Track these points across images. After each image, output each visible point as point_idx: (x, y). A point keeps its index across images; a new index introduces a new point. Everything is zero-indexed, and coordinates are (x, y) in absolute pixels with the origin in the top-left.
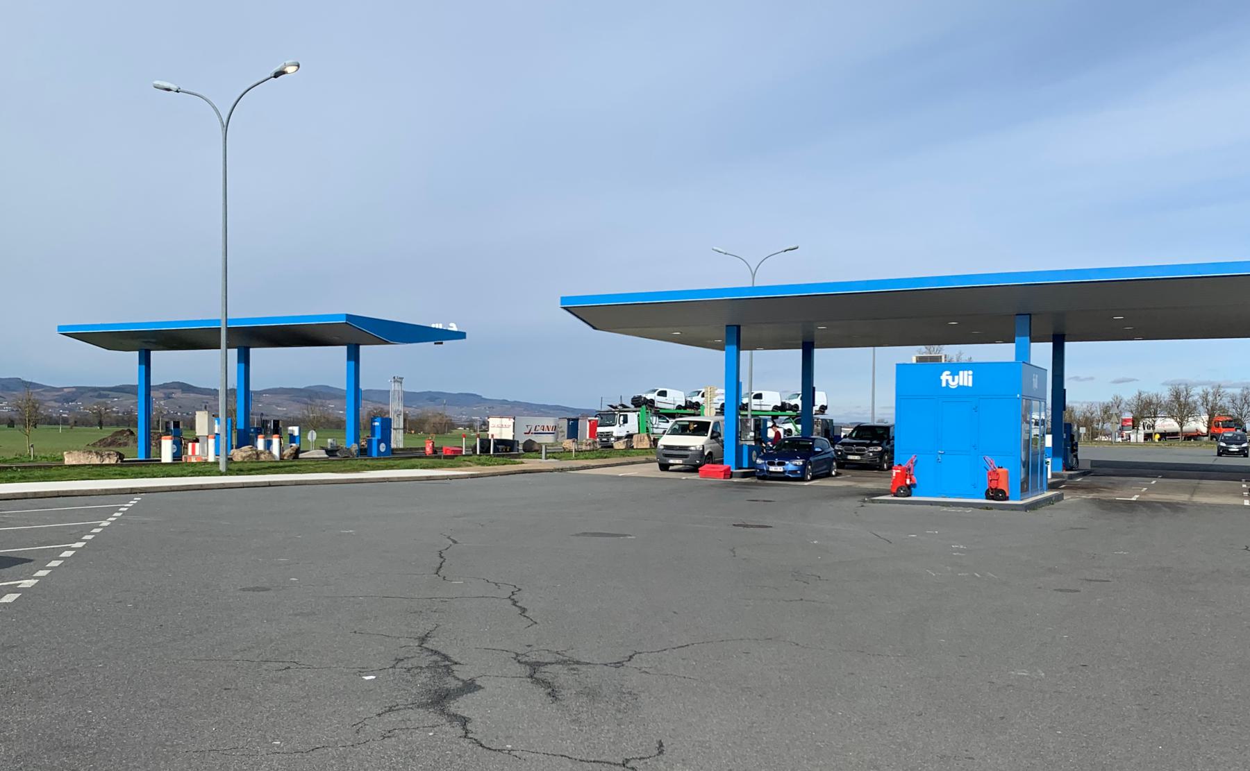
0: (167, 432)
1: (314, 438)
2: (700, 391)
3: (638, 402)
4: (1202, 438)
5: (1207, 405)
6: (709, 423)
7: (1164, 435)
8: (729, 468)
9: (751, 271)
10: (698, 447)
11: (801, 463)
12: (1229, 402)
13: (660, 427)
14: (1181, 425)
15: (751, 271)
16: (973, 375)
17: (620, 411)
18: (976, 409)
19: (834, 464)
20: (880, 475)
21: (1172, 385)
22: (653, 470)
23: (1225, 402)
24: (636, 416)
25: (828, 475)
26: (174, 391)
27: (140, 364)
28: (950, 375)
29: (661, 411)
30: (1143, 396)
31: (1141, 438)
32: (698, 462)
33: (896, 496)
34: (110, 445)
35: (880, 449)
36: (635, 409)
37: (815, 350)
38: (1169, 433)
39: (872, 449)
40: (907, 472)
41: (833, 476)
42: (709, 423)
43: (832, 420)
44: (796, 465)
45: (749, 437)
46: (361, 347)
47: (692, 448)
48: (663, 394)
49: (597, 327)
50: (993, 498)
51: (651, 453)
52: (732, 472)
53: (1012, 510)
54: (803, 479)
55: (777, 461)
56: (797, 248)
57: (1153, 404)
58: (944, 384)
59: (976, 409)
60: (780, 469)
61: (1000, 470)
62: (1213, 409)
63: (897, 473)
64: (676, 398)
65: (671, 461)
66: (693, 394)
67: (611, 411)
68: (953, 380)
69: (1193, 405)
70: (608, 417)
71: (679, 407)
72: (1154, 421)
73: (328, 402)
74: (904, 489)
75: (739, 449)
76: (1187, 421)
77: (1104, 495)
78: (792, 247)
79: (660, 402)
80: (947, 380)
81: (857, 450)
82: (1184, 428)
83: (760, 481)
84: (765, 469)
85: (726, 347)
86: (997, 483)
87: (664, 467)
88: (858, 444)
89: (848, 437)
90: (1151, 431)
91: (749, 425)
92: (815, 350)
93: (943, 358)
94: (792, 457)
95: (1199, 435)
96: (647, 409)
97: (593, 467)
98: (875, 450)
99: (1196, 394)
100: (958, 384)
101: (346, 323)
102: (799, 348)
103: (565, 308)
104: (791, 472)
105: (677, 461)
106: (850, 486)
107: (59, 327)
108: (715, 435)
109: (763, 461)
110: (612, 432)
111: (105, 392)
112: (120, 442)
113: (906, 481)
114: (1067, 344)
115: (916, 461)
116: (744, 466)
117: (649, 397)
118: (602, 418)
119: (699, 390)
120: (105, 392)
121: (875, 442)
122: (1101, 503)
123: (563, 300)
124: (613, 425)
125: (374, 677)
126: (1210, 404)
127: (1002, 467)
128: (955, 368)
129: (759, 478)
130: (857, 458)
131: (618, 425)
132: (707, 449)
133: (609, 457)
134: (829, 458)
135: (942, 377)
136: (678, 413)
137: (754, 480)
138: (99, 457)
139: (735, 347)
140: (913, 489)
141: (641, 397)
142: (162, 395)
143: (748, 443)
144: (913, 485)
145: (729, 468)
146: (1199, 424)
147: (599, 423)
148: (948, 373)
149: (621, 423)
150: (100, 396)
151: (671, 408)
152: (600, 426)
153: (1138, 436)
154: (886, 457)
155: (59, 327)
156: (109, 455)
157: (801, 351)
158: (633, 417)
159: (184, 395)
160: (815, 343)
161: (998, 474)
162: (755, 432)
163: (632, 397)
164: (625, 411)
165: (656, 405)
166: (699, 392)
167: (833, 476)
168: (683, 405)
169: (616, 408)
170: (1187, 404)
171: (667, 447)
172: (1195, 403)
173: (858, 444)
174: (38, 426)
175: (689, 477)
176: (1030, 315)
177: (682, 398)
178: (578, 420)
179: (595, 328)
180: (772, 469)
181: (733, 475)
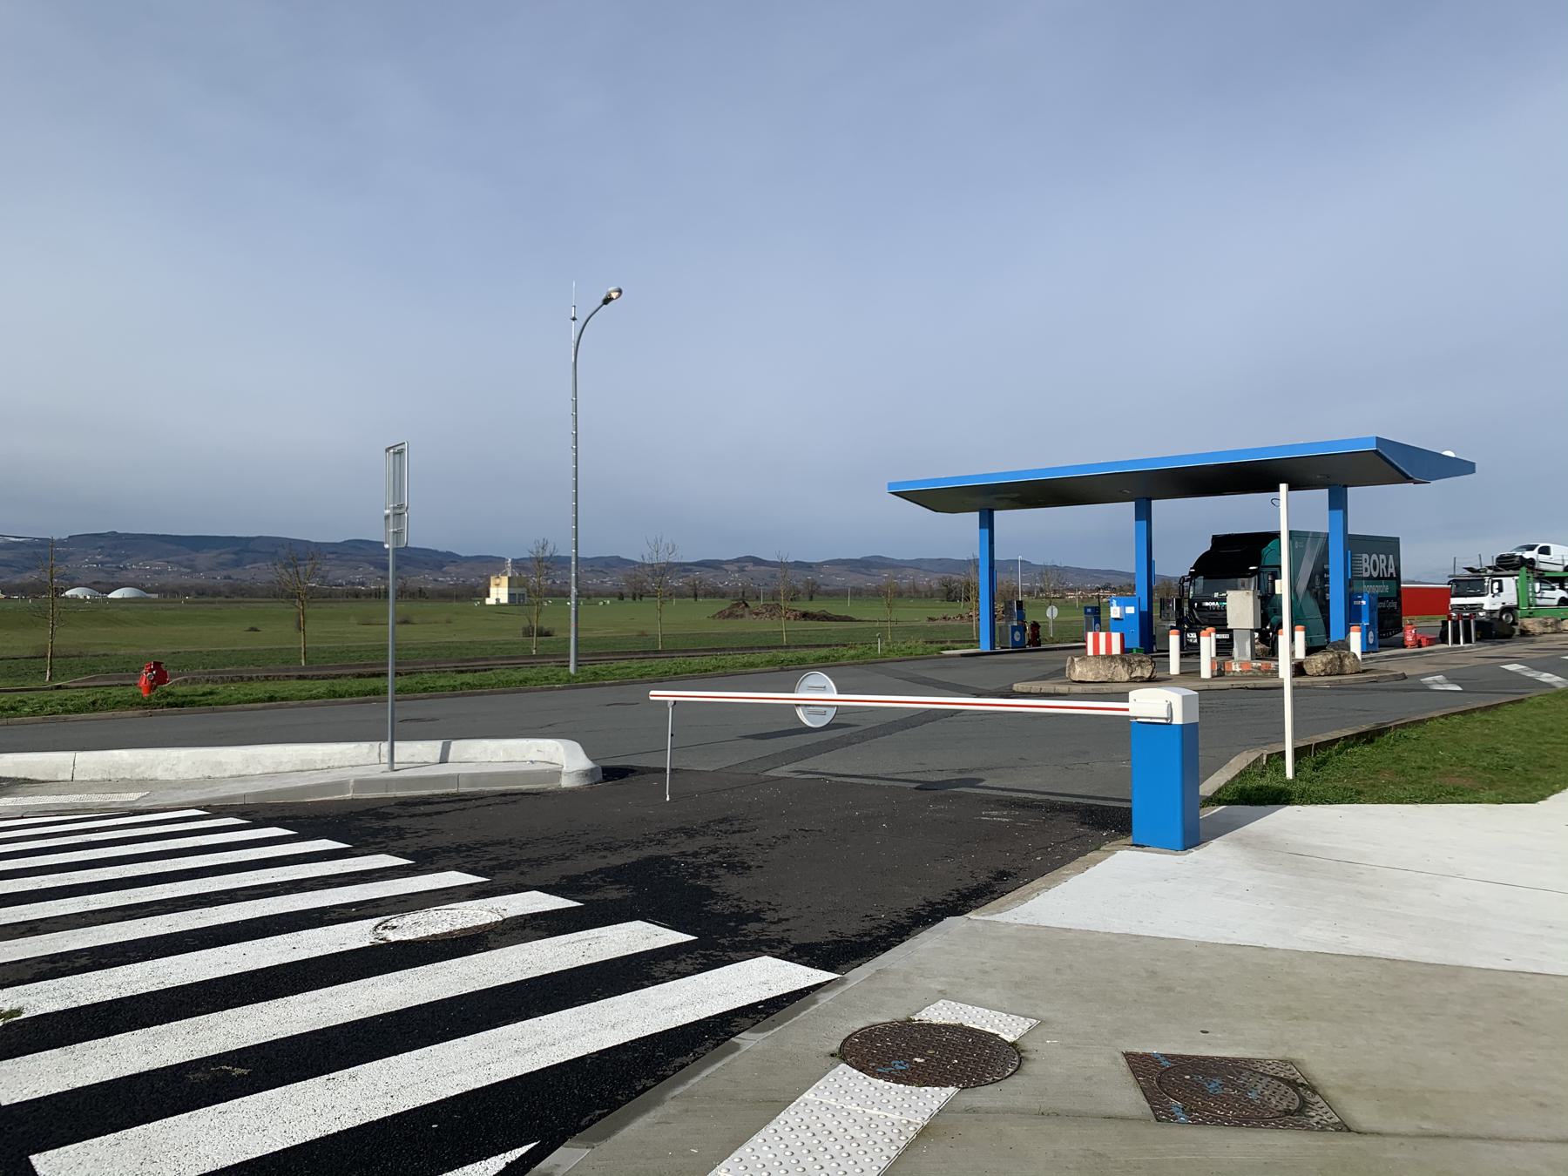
1: (1055, 615)
2: (1536, 546)
13: (1545, 596)
26: (747, 564)
27: (981, 527)
29: (1547, 575)
34: (728, 616)
46: (995, 512)
70: (1473, 583)
73: (882, 571)
101: (1376, 452)
102: (1144, 520)
103: (893, 493)
107: (889, 484)
110: (1482, 605)
111: (690, 567)
112: (738, 613)
117: (1528, 555)
120: (690, 567)
123: (890, 485)
124: (1483, 595)
131: (1490, 595)
138: (1126, 666)
141: (1513, 556)
142: (736, 568)
147: (1453, 593)
149: (1496, 591)
150: (685, 571)
155: (889, 484)
156: (1140, 662)
159: (756, 568)
174: (644, 599)
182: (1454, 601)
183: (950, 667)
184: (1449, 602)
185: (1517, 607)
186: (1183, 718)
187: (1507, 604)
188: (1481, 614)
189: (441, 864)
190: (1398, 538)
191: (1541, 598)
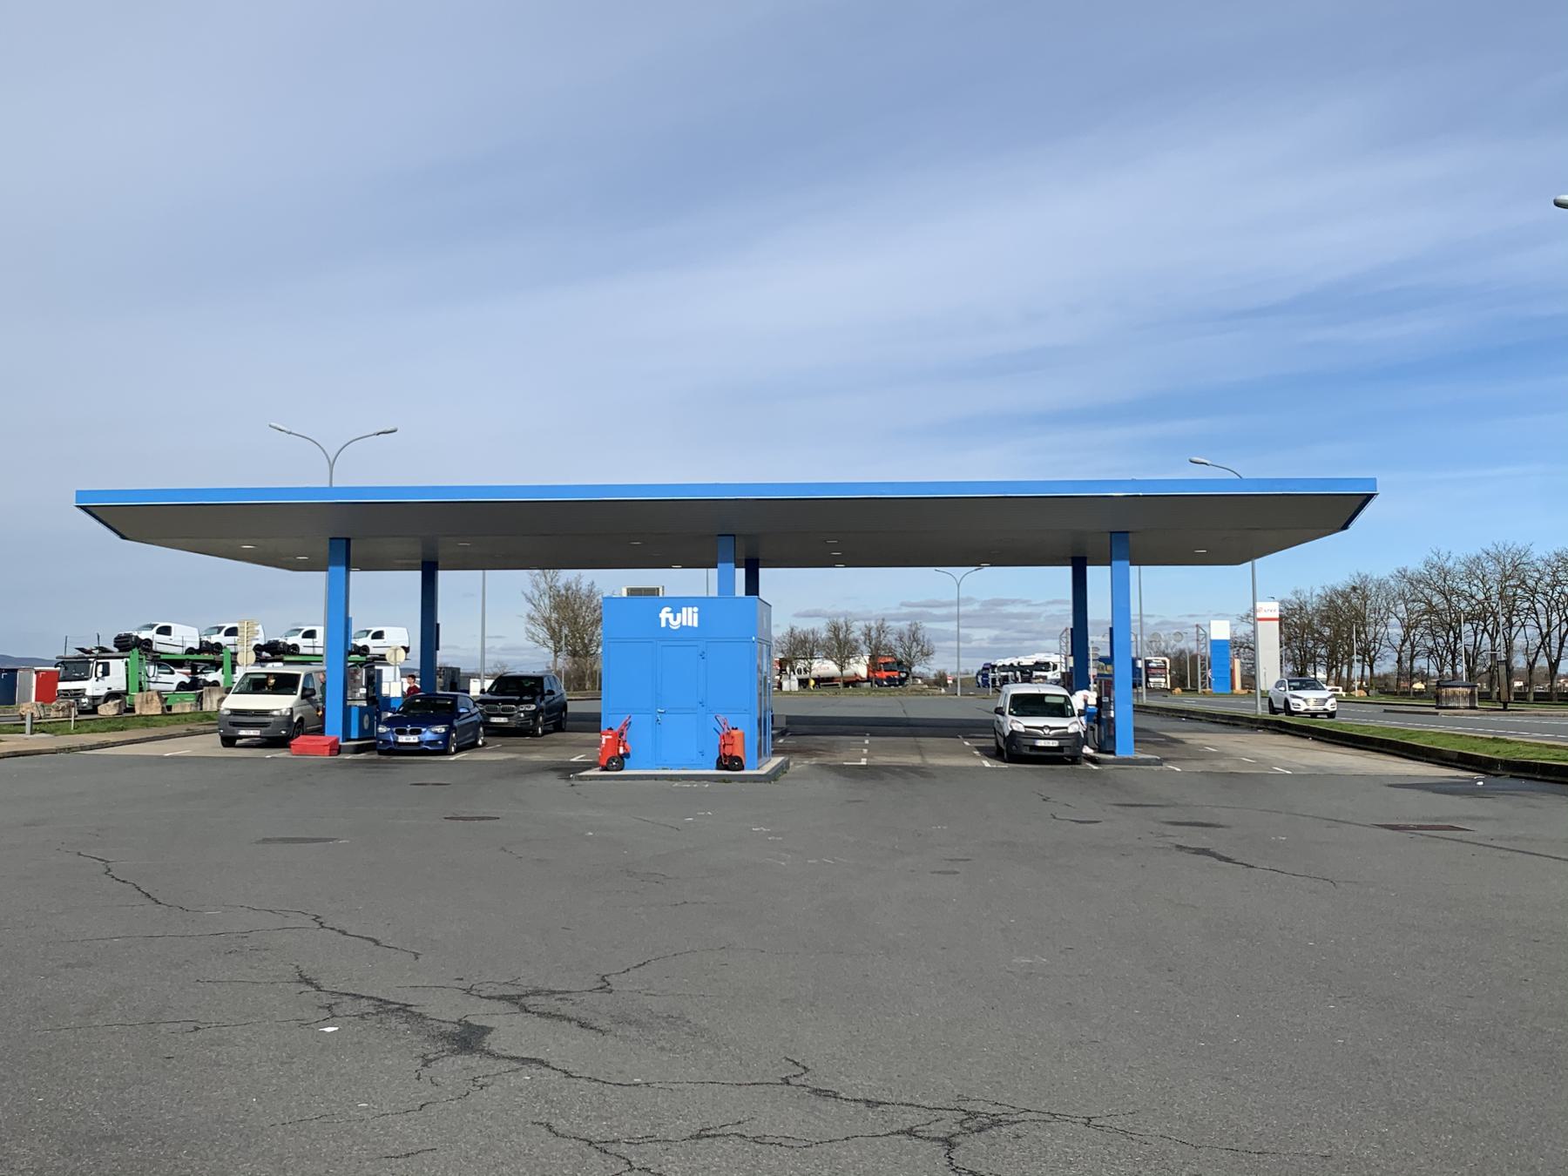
0: (489, 719)
2: (155, 625)
3: (125, 644)
4: (861, 684)
5: (870, 643)
6: (298, 676)
7: (818, 680)
8: (337, 740)
9: (329, 462)
10: (283, 711)
11: (443, 730)
12: (896, 640)
13: (159, 680)
14: (842, 668)
15: (329, 462)
16: (698, 612)
17: (97, 658)
18: (702, 656)
19: (481, 729)
20: (536, 743)
21: (829, 618)
22: (209, 745)
23: (890, 639)
24: (124, 664)
25: (474, 745)
28: (671, 612)
29: (163, 657)
30: (797, 631)
31: (795, 685)
32: (283, 732)
33: (605, 769)
35: (533, 707)
36: (121, 654)
37: (440, 572)
38: (823, 679)
39: (524, 707)
40: (619, 737)
41: (480, 746)
42: (298, 676)
43: (459, 669)
44: (436, 733)
45: (358, 695)
47: (275, 713)
48: (165, 631)
49: (128, 537)
50: (726, 768)
51: (186, 720)
52: (340, 746)
53: (755, 782)
54: (445, 752)
55: (409, 728)
56: (395, 431)
57: (809, 642)
58: (663, 624)
59: (702, 656)
60: (413, 739)
61: (734, 732)
62: (877, 648)
63: (607, 740)
64: (185, 637)
65: (243, 732)
66: (210, 632)
67: (84, 658)
68: (675, 619)
69: (854, 644)
70: (77, 666)
71: (191, 651)
72: (811, 664)
74: (616, 760)
75: (347, 711)
76: (849, 663)
77: (826, 759)
78: (389, 429)
79: (161, 643)
80: (667, 619)
81: (503, 710)
82: (844, 672)
83: (384, 757)
84: (392, 739)
85: (330, 568)
86: (733, 749)
87: (229, 741)
88: (504, 702)
89: (488, 691)
90: (807, 675)
91: (358, 677)
92: (440, 572)
93: (661, 590)
94: (429, 723)
95: (858, 681)
96: (140, 654)
97: (114, 744)
98: (527, 709)
99: (857, 634)
100: (681, 623)
103: (82, 508)
104: (430, 743)
105: (252, 733)
106: (514, 759)
108: (307, 693)
109: (389, 729)
110: (85, 690)
113: (618, 750)
114: (761, 570)
115: (630, 723)
116: (352, 737)
117: (143, 635)
118: (66, 669)
119: (220, 625)
121: (526, 698)
122: (840, 770)
124: (86, 679)
125: (336, 1029)
126: (874, 642)
127: (736, 729)
128: (677, 604)
129: (381, 753)
130: (502, 720)
131: (94, 678)
132: (297, 713)
133: (126, 729)
134: (475, 721)
135: (661, 615)
136: (189, 660)
137: (375, 756)
139: (344, 568)
140: (625, 759)
143: (358, 703)
144: (627, 755)
145: (337, 740)
146: (860, 668)
147: (61, 676)
148: (669, 609)
149: (100, 675)
151: (179, 652)
152: (64, 680)
153: (790, 684)
154: (541, 718)
157: (420, 573)
158: (117, 666)
160: (440, 564)
161: (733, 737)
162: (367, 687)
163: (116, 636)
164: (104, 658)
165: (154, 647)
166: (368, 632)
167: (480, 746)
168: (197, 646)
169: (90, 652)
170: (847, 642)
171: (235, 712)
172: (857, 641)
173: (504, 702)
175: (275, 755)
176: (734, 535)
177: (195, 637)
178: (16, 670)
179: (123, 537)
180: (402, 739)
181: (342, 750)
182: (62, 686)
183: (1533, 807)
184: (56, 686)
185: (126, 693)
186: (727, 562)
187: (113, 689)
188: (83, 700)
189: (280, 691)
190: (77, 491)
191: (155, 682)
